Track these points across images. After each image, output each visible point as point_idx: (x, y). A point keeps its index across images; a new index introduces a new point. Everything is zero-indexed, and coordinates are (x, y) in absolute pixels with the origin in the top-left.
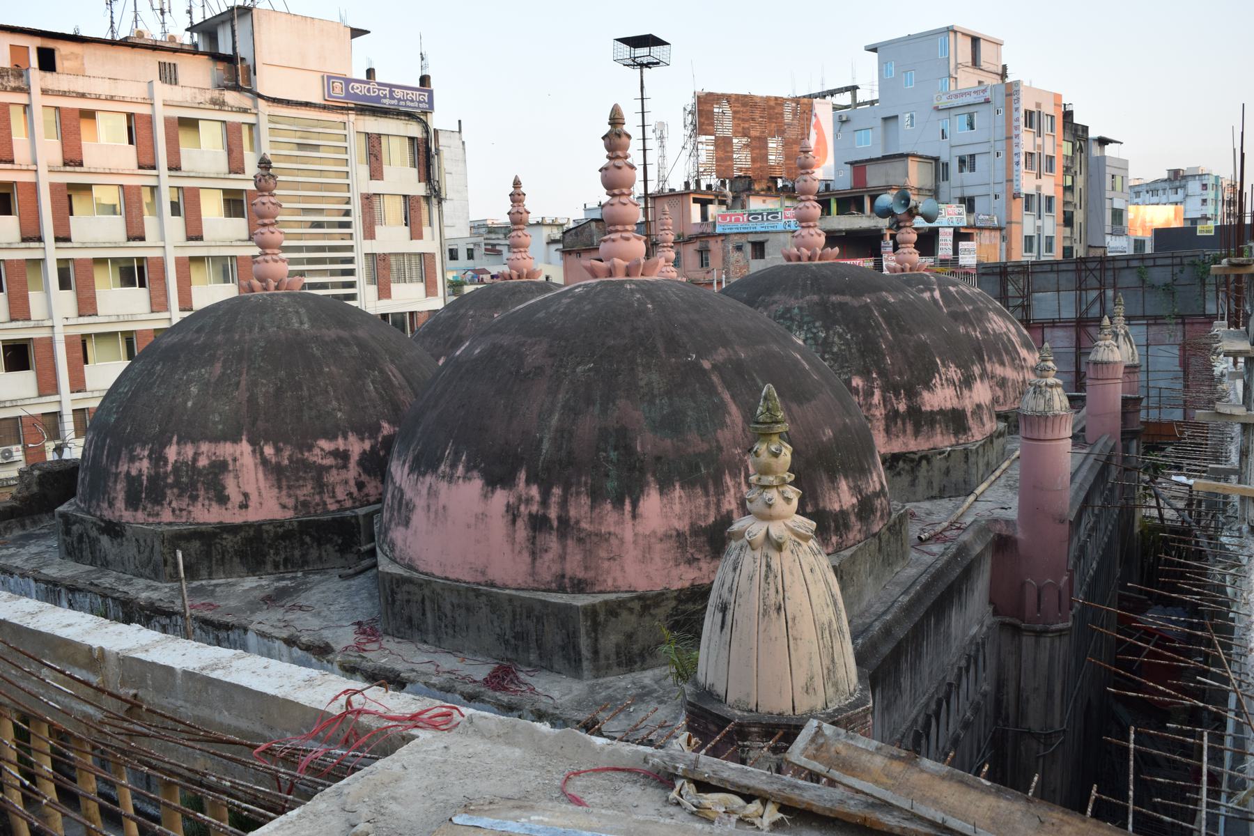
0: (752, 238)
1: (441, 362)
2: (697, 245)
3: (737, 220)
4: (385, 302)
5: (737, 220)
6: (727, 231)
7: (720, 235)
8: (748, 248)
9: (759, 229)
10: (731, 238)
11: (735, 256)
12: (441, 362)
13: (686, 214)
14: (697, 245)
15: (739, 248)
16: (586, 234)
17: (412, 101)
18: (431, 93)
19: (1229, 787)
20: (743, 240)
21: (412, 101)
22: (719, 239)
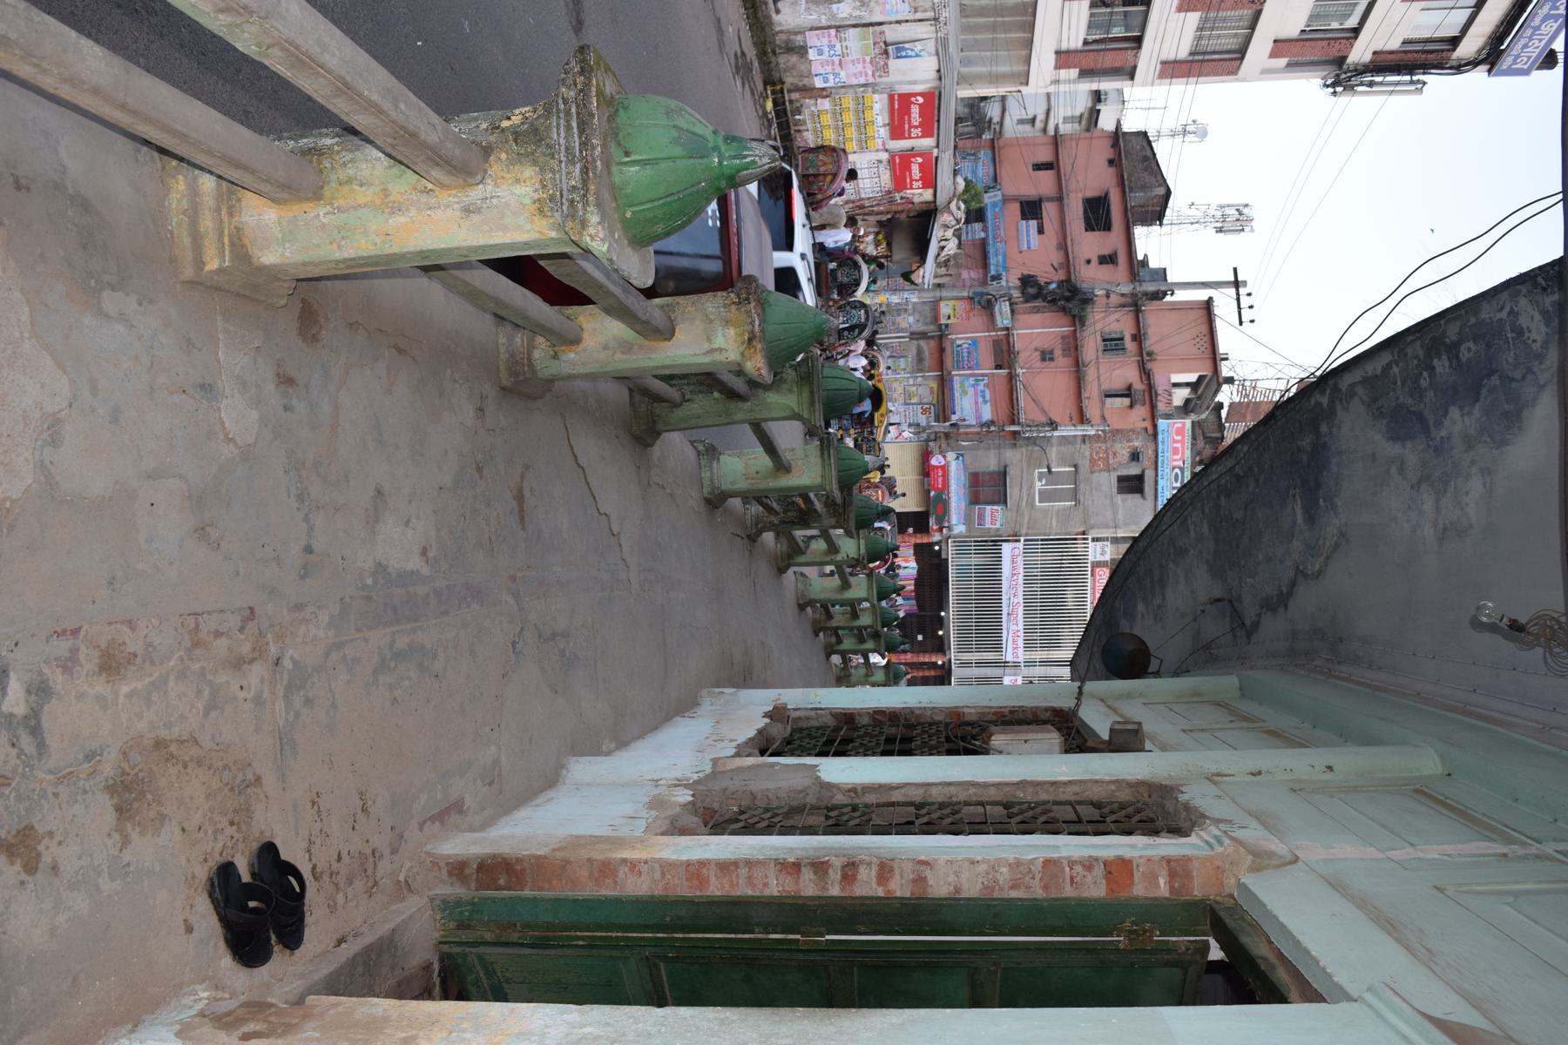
0: (1149, 475)
1: (252, 904)
2: (1138, 386)
3: (1175, 451)
4: (1051, 59)
5: (1175, 451)
6: (1160, 437)
7: (1155, 426)
8: (1134, 470)
9: (1161, 483)
10: (1151, 446)
11: (1123, 451)
12: (252, 904)
13: (1183, 363)
14: (1138, 386)
15: (1135, 456)
16: (1148, 179)
17: (1526, 46)
18: (1526, 72)
19: (794, 503)
20: (1146, 461)
21: (1526, 46)
22: (1147, 424)
